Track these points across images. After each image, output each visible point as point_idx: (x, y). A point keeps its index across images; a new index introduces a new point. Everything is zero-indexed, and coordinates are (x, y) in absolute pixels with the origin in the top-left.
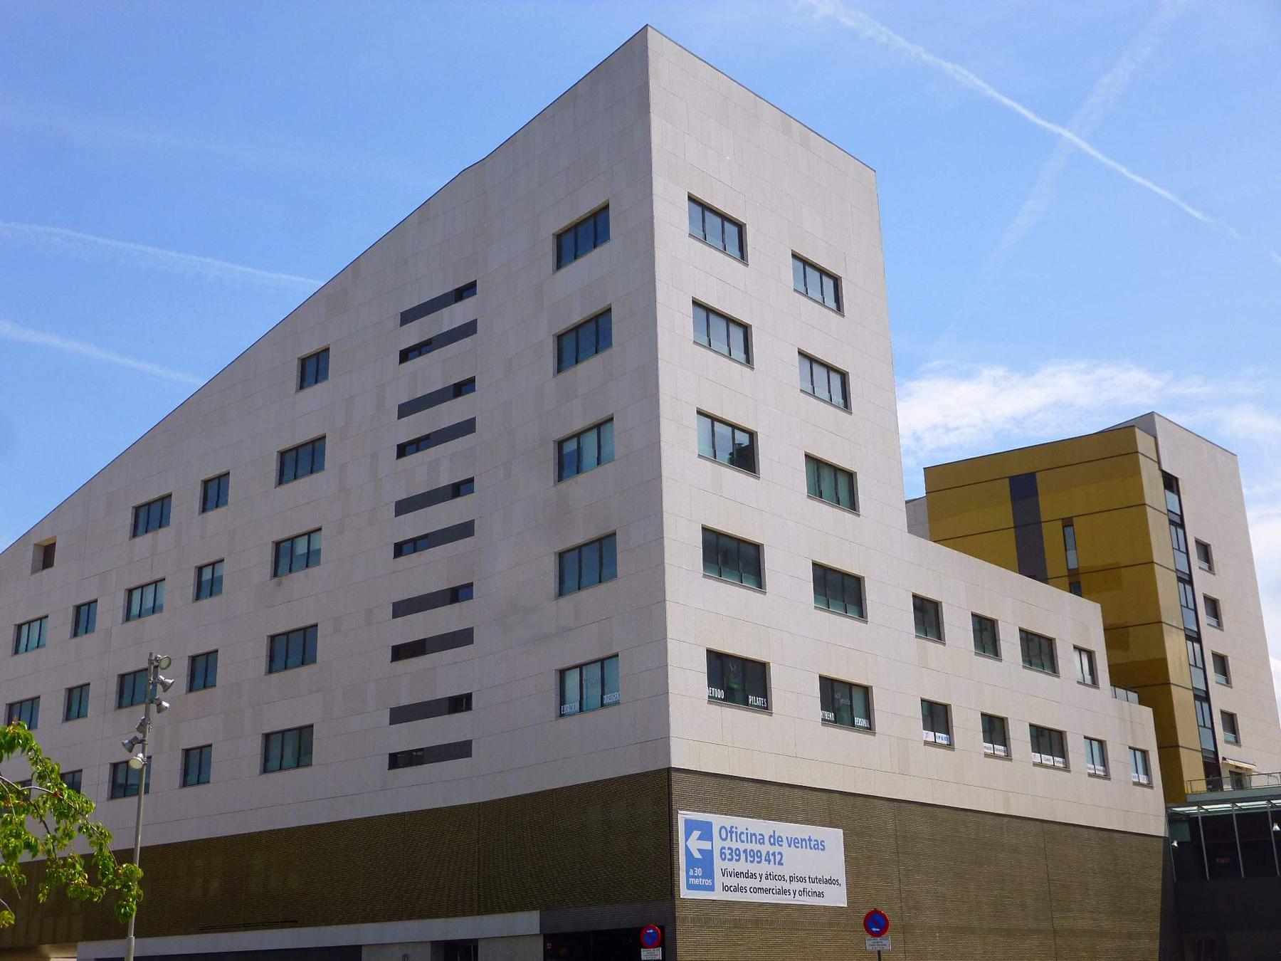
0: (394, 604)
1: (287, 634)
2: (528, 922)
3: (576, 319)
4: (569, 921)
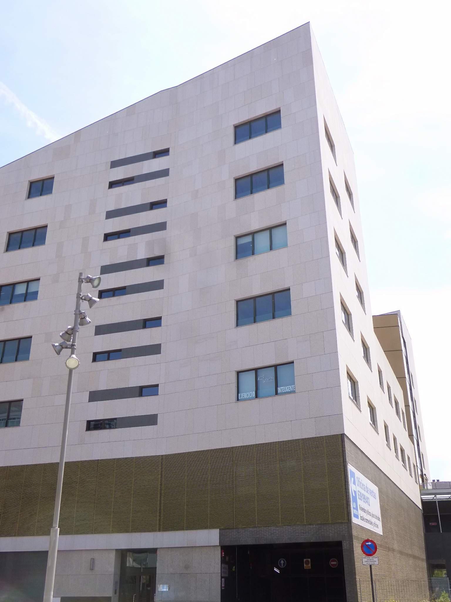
0: (96, 326)
1: (22, 232)
2: (211, 537)
3: (254, 168)
4: (247, 537)
